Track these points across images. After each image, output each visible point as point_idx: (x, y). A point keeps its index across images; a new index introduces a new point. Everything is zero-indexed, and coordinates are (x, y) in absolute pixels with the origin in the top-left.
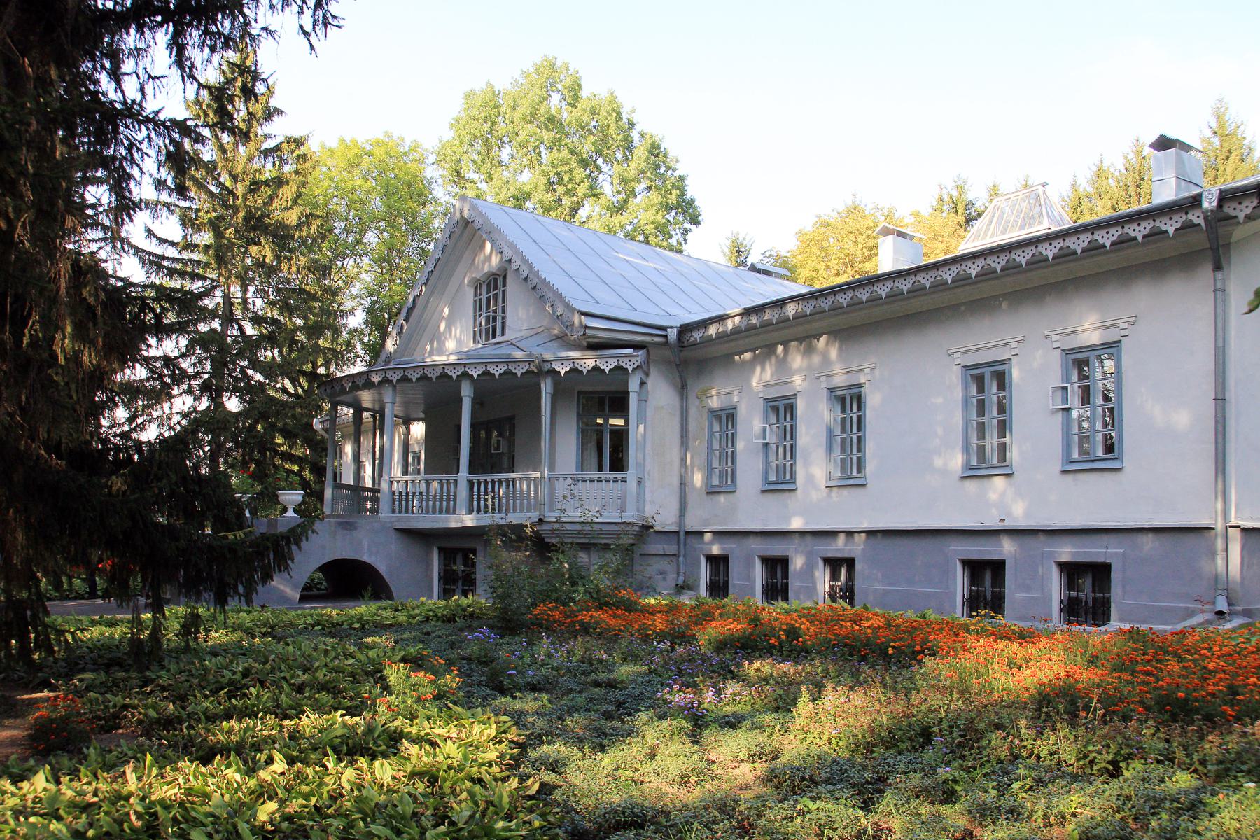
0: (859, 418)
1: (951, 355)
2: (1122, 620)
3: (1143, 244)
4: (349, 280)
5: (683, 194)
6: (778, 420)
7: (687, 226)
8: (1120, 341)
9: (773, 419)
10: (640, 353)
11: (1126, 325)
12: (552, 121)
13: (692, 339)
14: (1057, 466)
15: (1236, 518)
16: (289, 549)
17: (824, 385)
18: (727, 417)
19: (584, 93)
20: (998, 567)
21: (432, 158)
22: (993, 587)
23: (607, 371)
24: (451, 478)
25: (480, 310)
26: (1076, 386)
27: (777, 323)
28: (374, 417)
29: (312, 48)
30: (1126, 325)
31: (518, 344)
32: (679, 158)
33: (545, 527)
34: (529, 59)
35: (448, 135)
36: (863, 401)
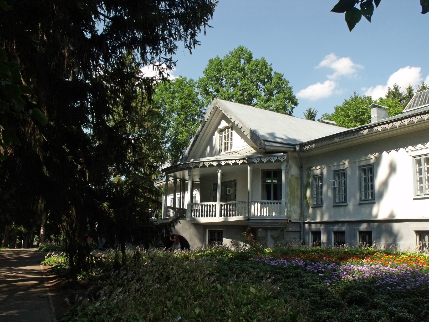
0: (345, 181)
1: (355, 162)
4: (165, 130)
5: (291, 95)
7: (293, 106)
9: (337, 178)
10: (286, 154)
12: (242, 70)
13: (305, 149)
16: (171, 228)
17: (357, 165)
18: (342, 174)
19: (254, 59)
20: (342, 233)
21: (197, 85)
22: (426, 243)
23: (215, 166)
24: (214, 203)
25: (222, 140)
27: (338, 142)
28: (180, 181)
29: (191, 52)
31: (238, 152)
32: (289, 81)
33: (250, 221)
34: (234, 47)
35: (203, 76)
36: (373, 170)
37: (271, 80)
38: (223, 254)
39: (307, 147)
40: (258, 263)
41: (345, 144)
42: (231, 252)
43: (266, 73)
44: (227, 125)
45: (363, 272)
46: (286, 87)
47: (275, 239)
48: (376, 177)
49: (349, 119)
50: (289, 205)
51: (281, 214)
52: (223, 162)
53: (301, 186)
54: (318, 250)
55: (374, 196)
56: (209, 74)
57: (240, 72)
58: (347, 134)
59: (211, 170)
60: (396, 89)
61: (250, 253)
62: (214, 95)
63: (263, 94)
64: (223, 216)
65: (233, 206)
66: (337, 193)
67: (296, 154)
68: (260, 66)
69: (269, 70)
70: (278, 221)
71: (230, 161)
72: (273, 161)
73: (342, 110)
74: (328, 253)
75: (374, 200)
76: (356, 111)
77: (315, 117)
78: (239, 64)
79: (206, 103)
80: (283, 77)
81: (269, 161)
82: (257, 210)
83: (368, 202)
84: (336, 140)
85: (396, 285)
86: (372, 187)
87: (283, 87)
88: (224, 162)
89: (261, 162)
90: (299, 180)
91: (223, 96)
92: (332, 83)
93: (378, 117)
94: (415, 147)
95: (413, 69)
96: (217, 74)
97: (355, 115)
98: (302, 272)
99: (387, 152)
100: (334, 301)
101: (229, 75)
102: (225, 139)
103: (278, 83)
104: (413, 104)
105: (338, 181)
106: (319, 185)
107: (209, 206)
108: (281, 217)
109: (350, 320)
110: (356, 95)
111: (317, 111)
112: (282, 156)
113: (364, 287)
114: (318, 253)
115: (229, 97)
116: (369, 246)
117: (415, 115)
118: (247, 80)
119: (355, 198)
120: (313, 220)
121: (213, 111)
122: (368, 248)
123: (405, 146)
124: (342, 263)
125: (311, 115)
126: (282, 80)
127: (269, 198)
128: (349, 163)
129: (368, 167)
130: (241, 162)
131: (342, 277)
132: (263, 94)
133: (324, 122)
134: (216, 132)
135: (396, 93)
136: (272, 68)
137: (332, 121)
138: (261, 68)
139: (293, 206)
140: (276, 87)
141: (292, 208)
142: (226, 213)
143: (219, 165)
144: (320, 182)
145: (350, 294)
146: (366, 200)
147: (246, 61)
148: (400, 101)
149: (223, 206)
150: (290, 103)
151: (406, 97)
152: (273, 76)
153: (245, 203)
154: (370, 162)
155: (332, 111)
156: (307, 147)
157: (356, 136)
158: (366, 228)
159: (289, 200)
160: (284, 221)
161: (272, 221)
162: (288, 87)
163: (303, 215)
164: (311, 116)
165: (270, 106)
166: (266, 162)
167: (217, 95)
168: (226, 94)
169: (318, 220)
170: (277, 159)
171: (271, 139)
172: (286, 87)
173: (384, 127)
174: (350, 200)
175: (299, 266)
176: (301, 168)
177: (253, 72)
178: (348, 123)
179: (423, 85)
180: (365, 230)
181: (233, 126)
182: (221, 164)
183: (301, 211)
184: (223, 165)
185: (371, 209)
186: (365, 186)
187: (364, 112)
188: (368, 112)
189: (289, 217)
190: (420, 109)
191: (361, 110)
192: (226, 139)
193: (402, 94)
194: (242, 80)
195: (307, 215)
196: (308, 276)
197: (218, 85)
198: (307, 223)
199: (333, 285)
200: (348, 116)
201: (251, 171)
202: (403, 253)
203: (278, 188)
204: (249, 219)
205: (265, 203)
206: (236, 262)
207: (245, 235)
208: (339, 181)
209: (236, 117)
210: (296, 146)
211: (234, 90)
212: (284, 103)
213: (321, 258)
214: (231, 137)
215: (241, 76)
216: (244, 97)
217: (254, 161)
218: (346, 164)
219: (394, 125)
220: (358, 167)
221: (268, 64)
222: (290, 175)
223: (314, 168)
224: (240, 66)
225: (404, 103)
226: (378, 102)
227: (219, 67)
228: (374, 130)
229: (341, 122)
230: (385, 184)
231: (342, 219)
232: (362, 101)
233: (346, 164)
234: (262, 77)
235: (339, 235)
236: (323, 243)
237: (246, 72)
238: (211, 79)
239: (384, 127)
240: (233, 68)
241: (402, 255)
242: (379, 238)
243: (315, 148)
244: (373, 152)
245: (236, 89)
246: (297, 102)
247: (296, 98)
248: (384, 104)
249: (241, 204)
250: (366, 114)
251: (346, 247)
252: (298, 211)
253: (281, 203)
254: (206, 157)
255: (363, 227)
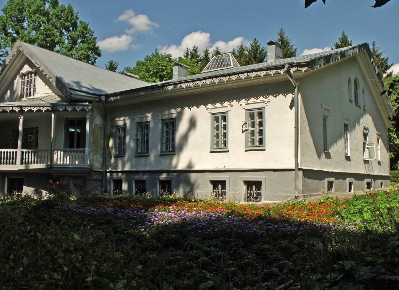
0: (147, 133)
1: (158, 116)
2: (265, 200)
3: (273, 76)
5: (95, 45)
6: (142, 130)
7: (96, 56)
8: (265, 107)
9: (140, 130)
11: (266, 102)
12: (47, 14)
13: (110, 100)
14: (244, 149)
15: (301, 166)
24: (14, 150)
25: (24, 85)
26: (250, 122)
30: (266, 102)
31: (42, 99)
32: (94, 32)
37: (76, 29)
38: (25, 202)
39: (112, 99)
40: (66, 211)
41: (150, 98)
42: (34, 201)
43: (71, 20)
44: (30, 70)
45: (173, 217)
46: (90, 37)
47: (79, 187)
48: (177, 130)
49: (150, 74)
50: (91, 154)
51: (84, 163)
52: (25, 109)
53: (104, 136)
54: (122, 197)
55: (175, 148)
56: (9, 14)
57: (44, 16)
58: (146, 90)
59: (13, 116)
60: (195, 50)
61: (56, 201)
62: (13, 37)
63: (66, 42)
64: (24, 164)
65: (34, 154)
66: (139, 144)
67: (101, 105)
68: (66, 12)
69: (75, 18)
70: (84, 169)
71: (34, 107)
72: (79, 110)
73: (143, 65)
74: (130, 201)
75: (175, 151)
76: (156, 67)
77: (116, 70)
78: (43, 7)
79: (4, 45)
80: (88, 27)
81: (74, 110)
82: (60, 159)
83: (169, 153)
84: (142, 93)
85: (206, 228)
86: (173, 139)
87: (87, 37)
88: (27, 108)
89: (66, 110)
90: (103, 130)
91: (24, 39)
92: (129, 37)
93: (179, 75)
94: (214, 105)
95: (204, 34)
96: (18, 15)
97: (155, 71)
98: (113, 219)
99: (189, 108)
100: (153, 245)
101: (31, 17)
102: (27, 84)
103: (83, 32)
104: (211, 66)
105: (140, 133)
106: (122, 135)
107: (9, 153)
108: (84, 166)
109: (173, 261)
110: (158, 52)
111: (118, 64)
112: (88, 105)
113: (177, 231)
114: (122, 200)
115: (30, 41)
116: (170, 195)
117: (217, 77)
118: (50, 25)
119: (156, 148)
120: (115, 169)
121: (15, 53)
122: (169, 196)
123: (205, 104)
124: (149, 210)
125: (112, 67)
126: (86, 30)
127: (71, 146)
128: (152, 116)
129: (170, 121)
130: (45, 109)
131: (154, 223)
132: (66, 42)
133: (128, 75)
134: (18, 77)
135: (194, 54)
136: (78, 17)
137: (134, 74)
138: (66, 15)
139: (96, 155)
140: (80, 36)
141: (94, 157)
142: (27, 160)
143: (22, 112)
144: (123, 133)
145: (164, 239)
146: (167, 151)
147: (52, 5)
148: (197, 62)
149: (24, 153)
150: (94, 54)
151: (202, 59)
152: (78, 25)
153: (48, 151)
154: (172, 116)
155: (133, 66)
156: (112, 99)
157: (161, 91)
158: (166, 177)
159: (92, 149)
160: (87, 170)
161: (75, 170)
162: (92, 37)
163: (105, 163)
164: (112, 68)
165: (73, 55)
166: (71, 110)
167: (17, 37)
168: (27, 37)
169: (120, 169)
170: (82, 108)
171: (77, 87)
172: (90, 37)
173: (188, 85)
174: (151, 151)
175: (108, 213)
176: (105, 118)
177: (58, 17)
178: (148, 78)
179: (218, 50)
180: (164, 179)
181: (38, 72)
182: (24, 110)
183: (104, 160)
184: (26, 111)
185: (171, 160)
186: (167, 138)
187: (164, 69)
188: (167, 69)
189: (92, 166)
190: (217, 71)
191: (160, 67)
192: (29, 85)
193: (199, 56)
194: (45, 25)
195: (109, 164)
196: (120, 223)
197: (18, 26)
198: (108, 172)
199: (147, 230)
200: (148, 71)
201: (55, 119)
202: (200, 201)
203: (82, 135)
204: (51, 167)
205: (68, 152)
206: (42, 211)
207: (52, 183)
208: (142, 133)
209: (41, 62)
210: (102, 97)
211: (36, 34)
212: (88, 52)
213: (129, 205)
214: (34, 82)
215: (45, 21)
216: (46, 42)
217: (59, 109)
218: (149, 117)
219: (197, 83)
220: (161, 120)
221: (74, 12)
222: (94, 125)
223: (118, 119)
224: (44, 10)
225: (200, 64)
226: (177, 60)
227: (21, 7)
228: (179, 87)
229: (141, 76)
230: (185, 137)
231: (143, 169)
232: (163, 58)
233: (149, 117)
234: (67, 24)
235: (140, 183)
236: (125, 191)
237: (50, 17)
238: (11, 19)
239: (188, 85)
240: (37, 10)
241: (200, 202)
242: (177, 187)
243: (121, 99)
244: (175, 107)
245: (39, 33)
246: (100, 53)
247: (100, 49)
248: (183, 63)
249: (43, 151)
250: (165, 71)
251: (148, 195)
252: (101, 159)
253: (84, 152)
254: (6, 102)
255: (164, 176)
